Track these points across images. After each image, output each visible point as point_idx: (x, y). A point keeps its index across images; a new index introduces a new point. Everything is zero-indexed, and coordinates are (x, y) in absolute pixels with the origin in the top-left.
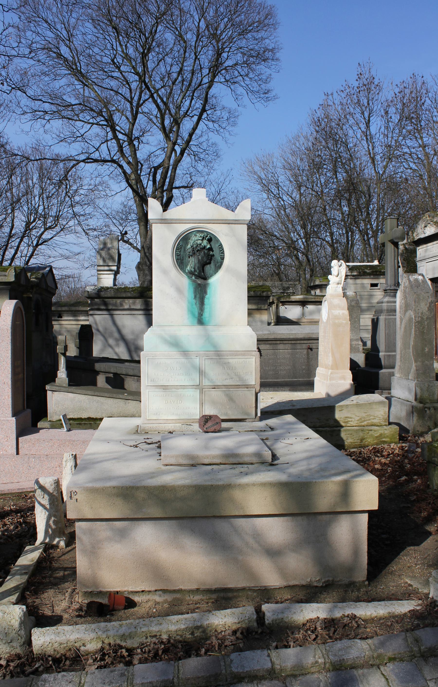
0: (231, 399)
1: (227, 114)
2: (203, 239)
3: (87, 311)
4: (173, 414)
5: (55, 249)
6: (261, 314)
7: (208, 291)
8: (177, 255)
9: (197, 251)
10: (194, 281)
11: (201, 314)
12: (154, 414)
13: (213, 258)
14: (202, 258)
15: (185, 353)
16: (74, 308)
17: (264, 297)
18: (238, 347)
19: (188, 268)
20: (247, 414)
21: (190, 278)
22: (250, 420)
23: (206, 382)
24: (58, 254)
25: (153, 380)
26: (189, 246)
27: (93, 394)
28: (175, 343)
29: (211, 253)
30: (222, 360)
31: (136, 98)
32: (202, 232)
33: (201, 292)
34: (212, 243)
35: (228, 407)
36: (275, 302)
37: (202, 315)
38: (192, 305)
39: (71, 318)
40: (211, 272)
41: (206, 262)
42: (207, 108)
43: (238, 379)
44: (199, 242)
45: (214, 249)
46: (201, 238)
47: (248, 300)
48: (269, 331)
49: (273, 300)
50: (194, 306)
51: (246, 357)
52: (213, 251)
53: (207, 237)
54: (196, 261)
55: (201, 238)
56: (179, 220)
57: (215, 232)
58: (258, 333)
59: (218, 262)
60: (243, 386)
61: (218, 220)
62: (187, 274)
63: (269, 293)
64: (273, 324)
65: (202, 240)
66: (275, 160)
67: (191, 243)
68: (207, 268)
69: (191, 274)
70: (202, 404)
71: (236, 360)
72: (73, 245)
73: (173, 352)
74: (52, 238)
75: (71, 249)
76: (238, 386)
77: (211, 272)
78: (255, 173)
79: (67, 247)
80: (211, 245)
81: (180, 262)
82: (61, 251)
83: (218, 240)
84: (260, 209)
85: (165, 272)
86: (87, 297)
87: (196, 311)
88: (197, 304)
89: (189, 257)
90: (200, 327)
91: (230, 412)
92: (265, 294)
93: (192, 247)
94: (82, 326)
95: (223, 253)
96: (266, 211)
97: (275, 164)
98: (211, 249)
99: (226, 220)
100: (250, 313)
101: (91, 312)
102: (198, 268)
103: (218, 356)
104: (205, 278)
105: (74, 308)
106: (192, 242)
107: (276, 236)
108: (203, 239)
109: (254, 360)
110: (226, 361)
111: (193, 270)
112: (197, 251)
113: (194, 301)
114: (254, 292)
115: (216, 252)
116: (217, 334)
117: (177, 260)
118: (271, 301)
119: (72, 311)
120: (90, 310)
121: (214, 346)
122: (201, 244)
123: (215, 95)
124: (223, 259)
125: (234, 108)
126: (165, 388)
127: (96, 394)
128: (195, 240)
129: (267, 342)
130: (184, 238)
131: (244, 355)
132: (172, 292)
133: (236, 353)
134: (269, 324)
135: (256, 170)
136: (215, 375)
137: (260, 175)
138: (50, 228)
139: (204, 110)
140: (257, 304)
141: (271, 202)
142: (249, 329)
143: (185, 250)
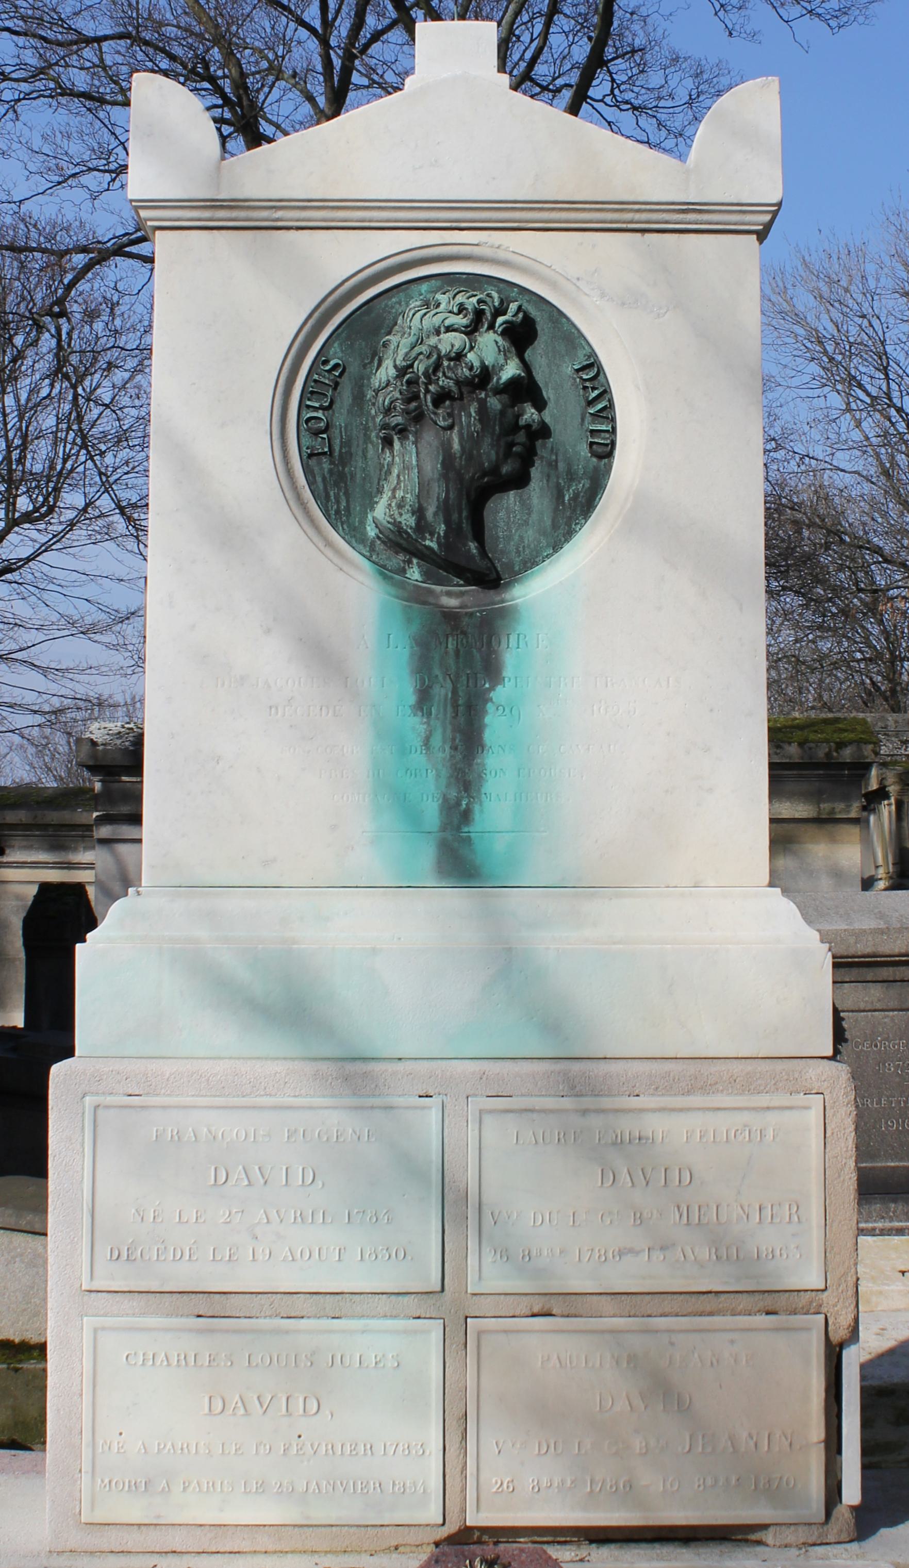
0: (663, 1390)
1: (689, 83)
3: (89, 828)
4: (262, 1488)
5: (46, 596)
6: (833, 840)
7: (511, 660)
8: (311, 428)
9: (438, 401)
10: (416, 597)
11: (458, 813)
12: (134, 1487)
13: (543, 449)
14: (471, 442)
15: (354, 1071)
16: (54, 816)
17: (843, 765)
18: (710, 1038)
19: (380, 511)
20: (772, 1490)
21: (384, 572)
22: (790, 1536)
23: (487, 1275)
24: (54, 617)
25: (125, 1255)
26: (386, 372)
27: (11, 1222)
28: (287, 1005)
29: (530, 414)
30: (595, 1121)
31: (343, 27)
33: (459, 662)
34: (537, 354)
35: (637, 1444)
36: (893, 789)
37: (466, 816)
38: (403, 751)
39: (42, 857)
41: (495, 470)
42: (609, 52)
43: (704, 1253)
44: (452, 341)
45: (548, 393)
46: (460, 321)
47: (774, 780)
48: (881, 916)
49: (882, 781)
50: (419, 759)
51: (763, 1100)
52: (540, 405)
53: (500, 311)
54: (433, 467)
55: (460, 321)
56: (323, 204)
57: (554, 285)
58: (827, 927)
59: (571, 476)
60: (744, 1302)
61: (571, 205)
62: (370, 551)
63: (868, 749)
64: (882, 884)
65: (471, 330)
66: (871, 268)
67: (399, 347)
68: (505, 509)
69: (400, 544)
70: (457, 1424)
71: (696, 1121)
72: (115, 585)
73: (271, 1064)
74: (29, 559)
75: (105, 599)
76: (703, 1302)
77: (530, 534)
78: (799, 319)
79: (90, 591)
81: (329, 473)
82: (66, 607)
83: (572, 338)
84: (819, 451)
85: (228, 535)
86: (90, 768)
87: (428, 791)
88: (437, 740)
89: (388, 442)
90: (455, 900)
91: (650, 1480)
92: (847, 754)
93: (402, 372)
94: (45, 887)
95: (607, 414)
96: (842, 459)
97: (872, 284)
98: (525, 390)
99: (622, 205)
100: (783, 837)
101: (104, 831)
102: (445, 508)
103: (579, 1090)
104: (490, 578)
105: (54, 816)
106: (406, 342)
107: (878, 550)
109: (814, 1117)
110: (627, 1126)
111: (408, 520)
112: (438, 401)
113: (414, 725)
114: (801, 745)
115: (562, 412)
116: (569, 942)
117: (309, 457)
118: (874, 785)
119: (44, 827)
120: (101, 821)
121: (552, 1026)
122: (459, 357)
123: (643, 11)
125: (713, 60)
126: (209, 1306)
127: (23, 1224)
128: (426, 328)
129: (870, 974)
130: (356, 324)
131: (748, 1086)
132: (271, 661)
133: (694, 1075)
134: (867, 884)
135: (800, 308)
136: (557, 1219)
137: (814, 323)
138: (28, 518)
139: (597, 61)
140: (816, 797)
141: (858, 424)
142: (782, 908)
143: (359, 398)
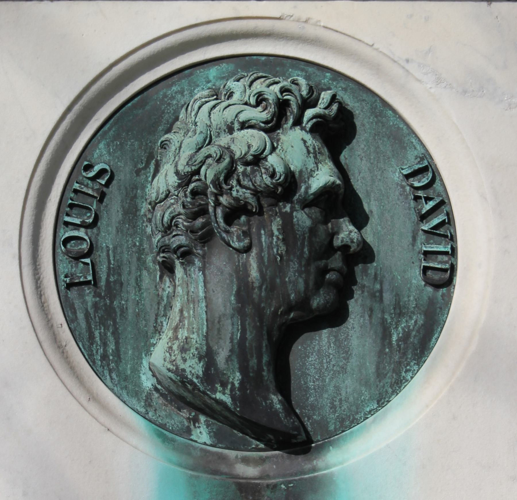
2: (280, 116)
9: (231, 217)
10: (204, 465)
13: (364, 275)
14: (273, 268)
21: (162, 431)
26: (166, 179)
29: (347, 232)
32: (274, 65)
34: (355, 156)
40: (348, 385)
41: (303, 303)
44: (252, 140)
45: (370, 206)
46: (259, 115)
52: (360, 220)
53: (307, 103)
54: (224, 300)
55: (259, 115)
57: (376, 69)
59: (400, 311)
65: (273, 127)
67: (181, 148)
68: (316, 354)
69: (184, 397)
80: (342, 171)
83: (399, 134)
89: (168, 268)
93: (185, 180)
95: (445, 231)
98: (342, 201)
102: (241, 352)
104: (298, 440)
106: (190, 143)
108: (280, 116)
111: (194, 368)
115: (389, 228)
117: (69, 286)
122: (257, 160)
124: (442, 279)
128: (215, 124)
130: (130, 113)
143: (131, 212)
